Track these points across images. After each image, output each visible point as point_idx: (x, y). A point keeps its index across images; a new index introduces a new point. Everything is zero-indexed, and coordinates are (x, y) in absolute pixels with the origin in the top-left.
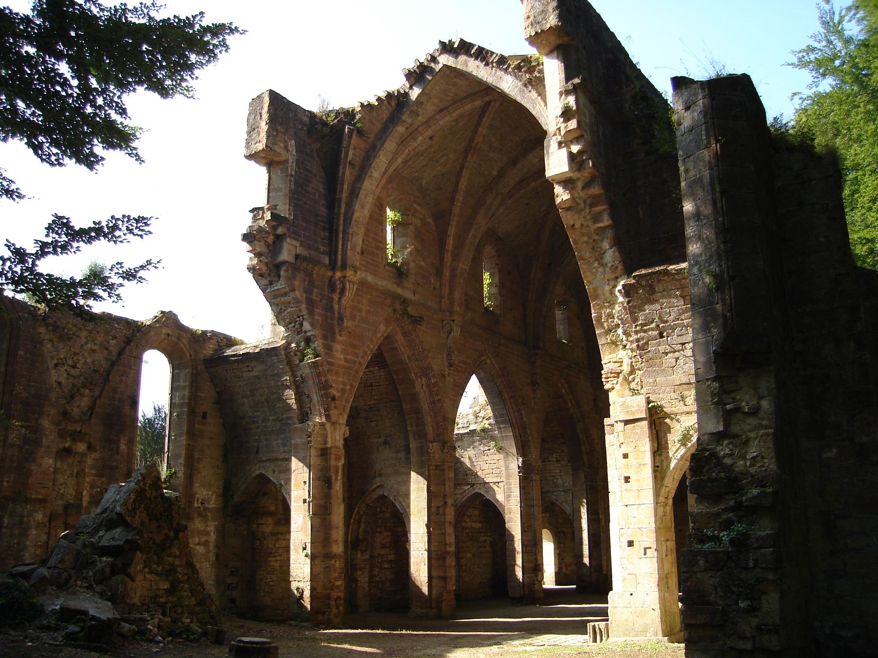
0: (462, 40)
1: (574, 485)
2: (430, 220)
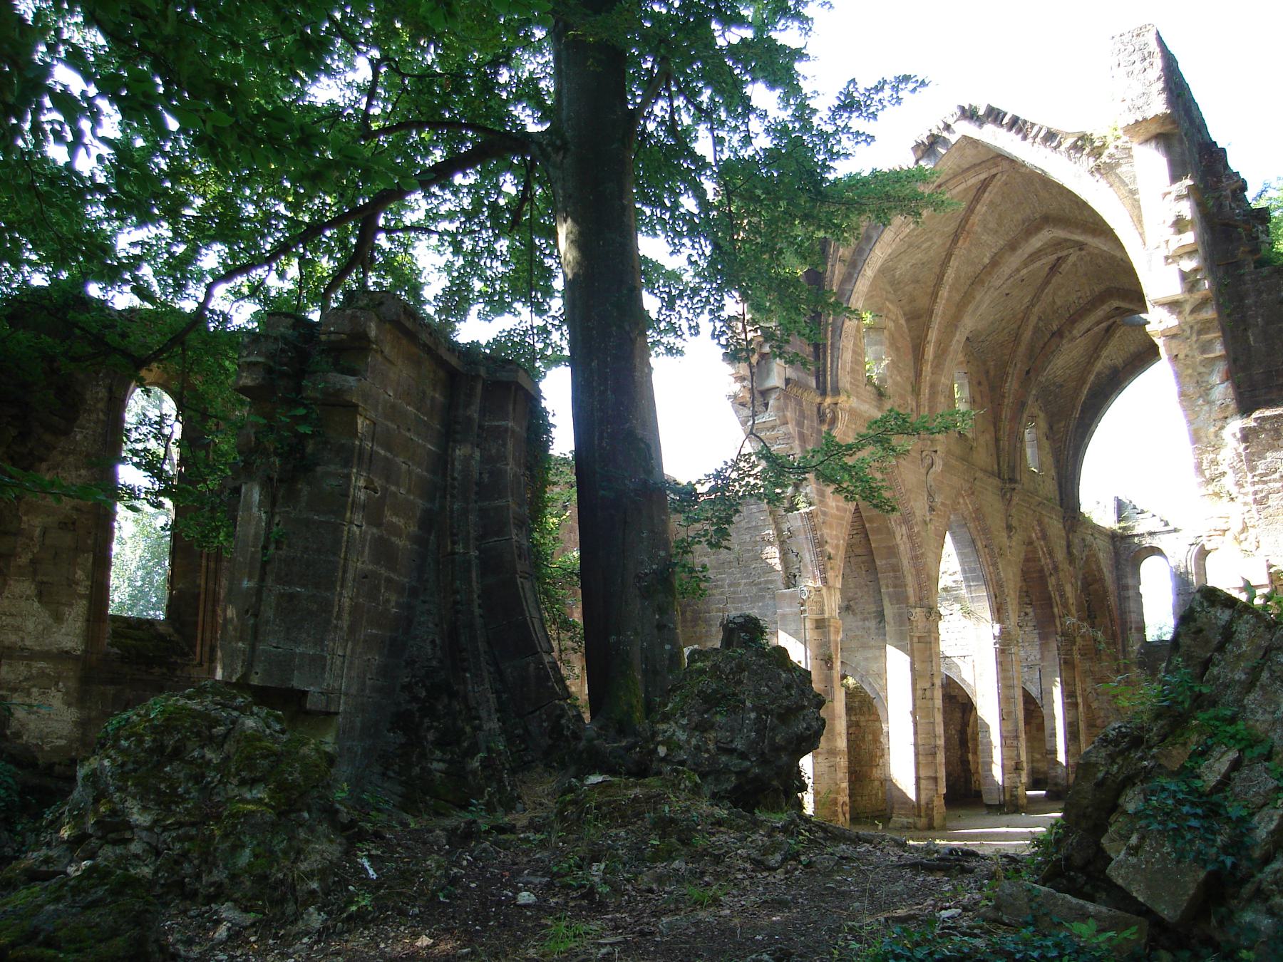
0: (989, 106)
1: (1042, 659)
2: (902, 321)
